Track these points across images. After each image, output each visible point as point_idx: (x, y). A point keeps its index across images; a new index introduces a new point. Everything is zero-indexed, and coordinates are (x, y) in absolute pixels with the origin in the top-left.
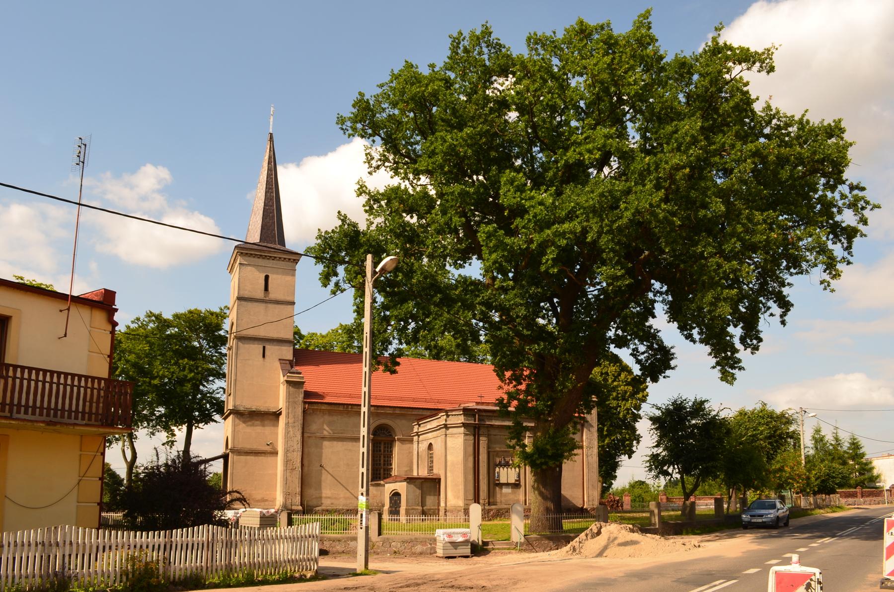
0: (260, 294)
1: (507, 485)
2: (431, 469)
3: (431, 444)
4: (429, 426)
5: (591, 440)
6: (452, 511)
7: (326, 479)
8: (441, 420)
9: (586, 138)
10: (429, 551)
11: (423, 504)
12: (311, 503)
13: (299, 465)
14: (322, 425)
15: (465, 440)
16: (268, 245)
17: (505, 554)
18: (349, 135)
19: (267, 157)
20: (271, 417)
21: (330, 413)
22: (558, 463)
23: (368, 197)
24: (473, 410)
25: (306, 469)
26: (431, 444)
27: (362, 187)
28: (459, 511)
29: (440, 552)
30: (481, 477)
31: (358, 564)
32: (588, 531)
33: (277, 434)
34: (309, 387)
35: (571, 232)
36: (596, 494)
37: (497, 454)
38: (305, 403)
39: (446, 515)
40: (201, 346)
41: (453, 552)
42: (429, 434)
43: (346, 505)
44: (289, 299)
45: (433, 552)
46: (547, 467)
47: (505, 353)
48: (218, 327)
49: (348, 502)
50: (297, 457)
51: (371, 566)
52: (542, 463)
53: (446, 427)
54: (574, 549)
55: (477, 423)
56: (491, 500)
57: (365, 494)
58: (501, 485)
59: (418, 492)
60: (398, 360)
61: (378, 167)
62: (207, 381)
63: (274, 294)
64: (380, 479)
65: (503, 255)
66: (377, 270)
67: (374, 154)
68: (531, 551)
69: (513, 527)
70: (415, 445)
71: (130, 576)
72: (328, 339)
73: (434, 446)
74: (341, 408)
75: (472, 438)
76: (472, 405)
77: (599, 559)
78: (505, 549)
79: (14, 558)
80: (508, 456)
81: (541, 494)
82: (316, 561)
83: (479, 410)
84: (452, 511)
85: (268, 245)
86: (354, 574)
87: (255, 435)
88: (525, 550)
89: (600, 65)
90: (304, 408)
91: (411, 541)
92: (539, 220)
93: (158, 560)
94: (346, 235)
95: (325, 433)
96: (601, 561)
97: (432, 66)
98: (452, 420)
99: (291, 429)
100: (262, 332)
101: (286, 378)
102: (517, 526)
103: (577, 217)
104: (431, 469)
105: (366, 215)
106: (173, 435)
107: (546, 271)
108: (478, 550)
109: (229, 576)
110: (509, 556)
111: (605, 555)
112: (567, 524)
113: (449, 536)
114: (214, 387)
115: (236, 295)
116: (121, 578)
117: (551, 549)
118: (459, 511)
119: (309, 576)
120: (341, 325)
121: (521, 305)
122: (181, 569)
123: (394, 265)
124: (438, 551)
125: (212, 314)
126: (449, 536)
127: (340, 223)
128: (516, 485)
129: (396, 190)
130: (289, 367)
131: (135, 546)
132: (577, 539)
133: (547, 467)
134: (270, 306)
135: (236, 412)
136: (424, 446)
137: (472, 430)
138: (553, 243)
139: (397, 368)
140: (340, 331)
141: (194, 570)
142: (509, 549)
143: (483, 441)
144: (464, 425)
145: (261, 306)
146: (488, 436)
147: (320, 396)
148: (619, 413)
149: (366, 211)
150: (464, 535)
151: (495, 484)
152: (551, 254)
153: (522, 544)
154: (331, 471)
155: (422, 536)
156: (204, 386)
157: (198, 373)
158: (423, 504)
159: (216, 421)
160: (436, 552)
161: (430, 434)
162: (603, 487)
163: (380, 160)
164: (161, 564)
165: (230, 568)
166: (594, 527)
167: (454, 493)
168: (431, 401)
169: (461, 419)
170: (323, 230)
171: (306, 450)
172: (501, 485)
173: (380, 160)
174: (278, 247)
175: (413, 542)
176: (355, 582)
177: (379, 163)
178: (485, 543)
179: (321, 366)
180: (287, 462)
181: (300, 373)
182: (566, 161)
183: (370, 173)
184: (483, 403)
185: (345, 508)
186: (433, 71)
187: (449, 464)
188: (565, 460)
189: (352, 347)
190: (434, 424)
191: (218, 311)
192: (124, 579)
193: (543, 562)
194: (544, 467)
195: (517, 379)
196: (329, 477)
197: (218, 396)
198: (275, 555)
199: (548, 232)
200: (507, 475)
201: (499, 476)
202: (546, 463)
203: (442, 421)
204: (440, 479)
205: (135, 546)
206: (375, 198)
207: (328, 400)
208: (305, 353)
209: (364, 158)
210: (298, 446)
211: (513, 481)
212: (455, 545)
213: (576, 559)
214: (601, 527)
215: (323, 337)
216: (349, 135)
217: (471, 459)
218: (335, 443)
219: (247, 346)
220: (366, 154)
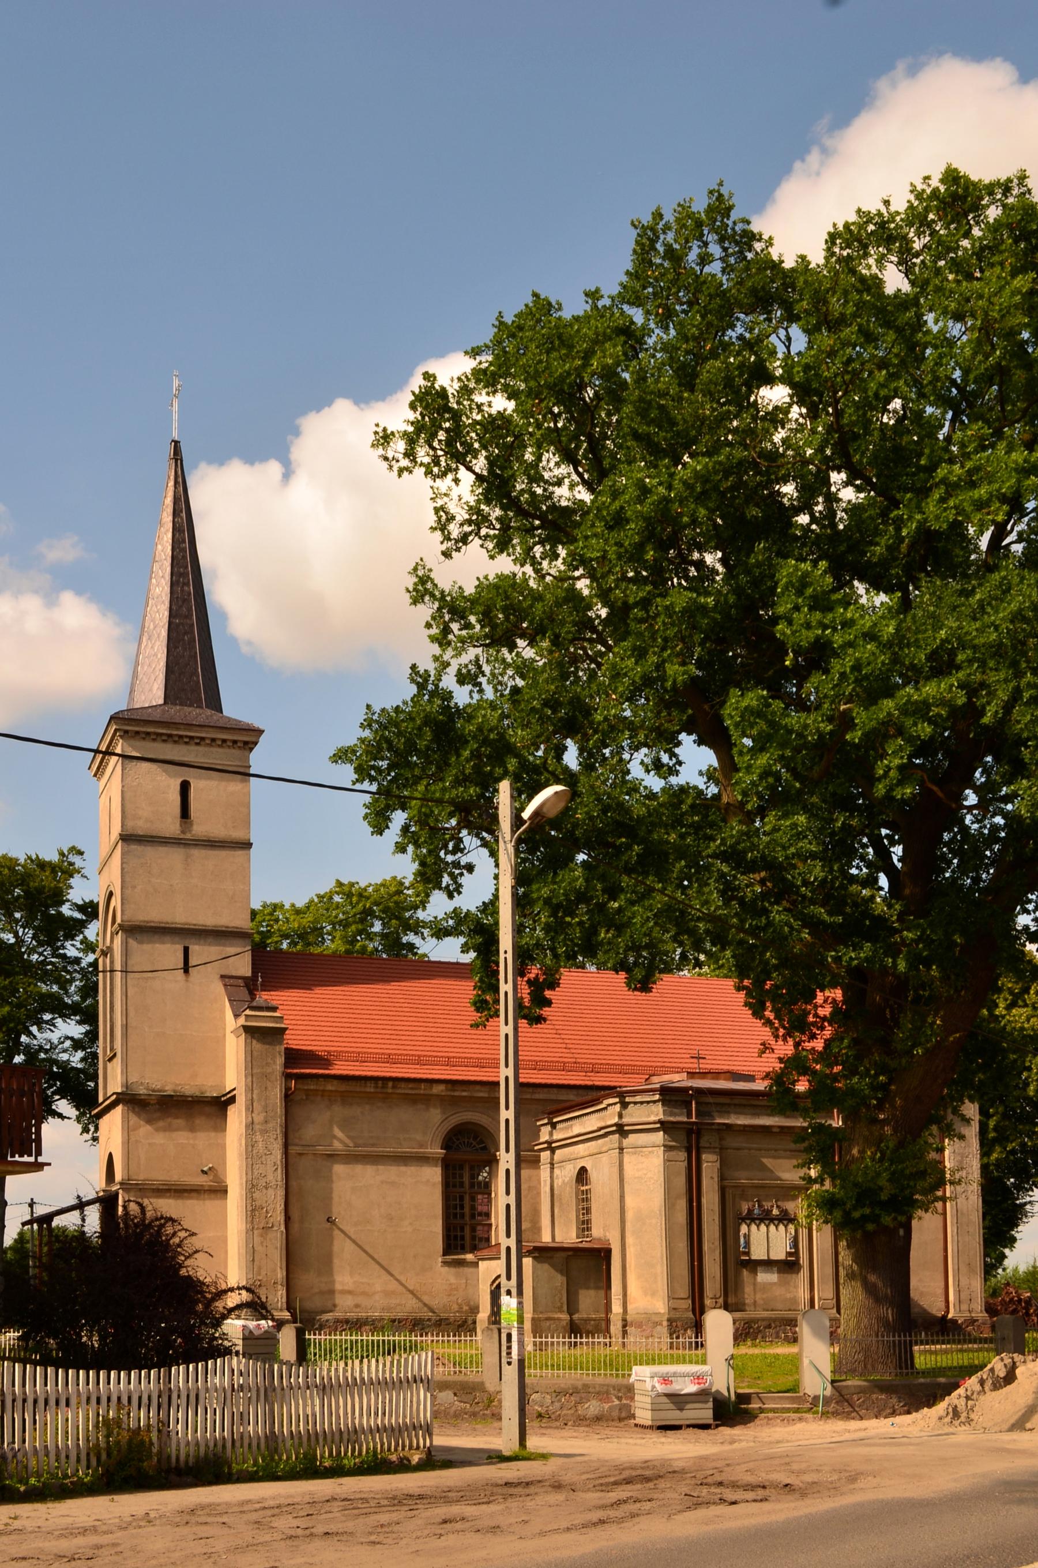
0: (171, 826)
1: (768, 1264)
2: (585, 1226)
3: (583, 1171)
4: (577, 1128)
5: (964, 1156)
6: (639, 1325)
7: (343, 1250)
8: (609, 1114)
9: (970, 473)
10: (615, 1414)
11: (572, 1307)
12: (309, 1305)
13: (280, 1218)
14: (330, 1128)
15: (666, 1161)
16: (188, 716)
17: (790, 1421)
18: (401, 471)
19: (169, 500)
20: (208, 1109)
21: (346, 1098)
22: (902, 1219)
23: (436, 605)
24: (684, 1090)
25: (295, 1227)
26: (583, 1171)
27: (424, 580)
28: (657, 1324)
29: (644, 1415)
30: (706, 1247)
31: (505, 1440)
32: (984, 1373)
33: (223, 1147)
34: (294, 1040)
35: (942, 702)
36: (976, 1285)
37: (743, 1192)
38: (288, 1077)
39: (625, 1333)
40: (20, 941)
41: (674, 1416)
42: (579, 1142)
43: (389, 1309)
44: (237, 834)
45: (624, 1416)
46: (876, 1229)
47: (767, 962)
48: (58, 897)
49: (393, 1301)
50: (274, 1201)
51: (534, 1443)
52: (864, 1218)
53: (621, 1130)
54: (956, 1414)
55: (697, 1120)
56: (731, 1300)
57: (514, 1291)
58: (754, 1265)
59: (560, 1280)
60: (548, 993)
61: (464, 539)
62: (39, 1023)
63: (202, 826)
64: (463, 1250)
65: (782, 757)
66: (526, 815)
67: (453, 508)
68: (847, 1416)
69: (806, 1362)
70: (544, 1172)
71: (104, 1456)
72: (309, 917)
73: (593, 1174)
74: (370, 1088)
75: (683, 1155)
76: (678, 1079)
77: (1016, 1435)
78: (788, 1410)
79: (24, 1420)
80: (768, 1198)
81: (870, 1290)
82: (428, 1430)
83: (700, 1092)
84: (639, 1325)
85: (188, 716)
86: (497, 1457)
87: (172, 1151)
88: (835, 1414)
89: (1003, 300)
90: (287, 1089)
91: (575, 1391)
92: (866, 677)
93: (149, 1425)
94: (428, 720)
95: (337, 1145)
96: (1022, 1439)
97: (593, 295)
98: (635, 1115)
99: (258, 1137)
100: (180, 916)
101: (242, 1021)
102: (815, 1358)
103: (959, 668)
104: (585, 1226)
105: (436, 649)
107: (889, 797)
108: (731, 1411)
109: (272, 1459)
110: (799, 1426)
111: (1028, 1426)
112: (927, 1356)
113: (666, 1380)
114: (55, 1037)
115: (117, 830)
116: (88, 1460)
117: (894, 1413)
118: (657, 1324)
119: (415, 1459)
120: (340, 884)
121: (813, 856)
122: (188, 1443)
123: (561, 805)
124: (638, 1413)
125: (42, 865)
126: (666, 1380)
127: (413, 689)
128: (789, 1266)
129: (505, 586)
130: (244, 993)
131: (109, 1399)
132: (961, 1391)
133: (876, 1229)
134: (196, 853)
135: (128, 1099)
136: (566, 1174)
137: (683, 1136)
138: (900, 732)
139: (546, 1012)
140: (337, 899)
141: (211, 1444)
142: (797, 1411)
143: (710, 1164)
144: (664, 1126)
145: (174, 857)
146: (722, 1151)
147: (325, 1061)
148: (1027, 1084)
149: (433, 639)
150: (698, 1378)
151: (739, 1263)
152: (894, 758)
153: (827, 1401)
154: (351, 1231)
155: (600, 1380)
156: (30, 1034)
157: (19, 1006)
158: (572, 1307)
159: (61, 1116)
160: (633, 1416)
161: (580, 1147)
162: (986, 1264)
163: (469, 522)
164: (154, 1436)
165: (272, 1441)
166: (998, 1365)
167: (643, 1284)
168: (576, 1067)
169: (657, 1113)
170: (377, 708)
171: (293, 1183)
172: (754, 1265)
173: (469, 522)
174: (204, 715)
175: (580, 1393)
176: (521, 1474)
177: (467, 529)
178: (744, 1398)
179: (318, 990)
180: (253, 1211)
181: (274, 1009)
182: (921, 524)
183: (447, 554)
184: (704, 1075)
185: (387, 1315)
186: (595, 307)
187: (629, 1215)
188: (920, 1212)
189: (370, 937)
190: (591, 1123)
191: (53, 857)
192: (94, 1462)
193: (891, 1440)
194: (870, 1227)
195: (798, 1026)
196: (349, 1246)
197: (64, 1057)
198: (338, 1417)
199: (888, 704)
200: (767, 1241)
201: (748, 1244)
202: (875, 1219)
203: (611, 1117)
204: (608, 1252)
205: (109, 1399)
206: (453, 608)
207: (340, 1068)
208: (278, 958)
209: (432, 519)
210: (276, 1177)
212: (678, 1400)
213: (962, 1435)
214: (1014, 1366)
215: (298, 912)
216: (401, 471)
217: (682, 1204)
218: (359, 1168)
219: (147, 947)
220: (437, 510)
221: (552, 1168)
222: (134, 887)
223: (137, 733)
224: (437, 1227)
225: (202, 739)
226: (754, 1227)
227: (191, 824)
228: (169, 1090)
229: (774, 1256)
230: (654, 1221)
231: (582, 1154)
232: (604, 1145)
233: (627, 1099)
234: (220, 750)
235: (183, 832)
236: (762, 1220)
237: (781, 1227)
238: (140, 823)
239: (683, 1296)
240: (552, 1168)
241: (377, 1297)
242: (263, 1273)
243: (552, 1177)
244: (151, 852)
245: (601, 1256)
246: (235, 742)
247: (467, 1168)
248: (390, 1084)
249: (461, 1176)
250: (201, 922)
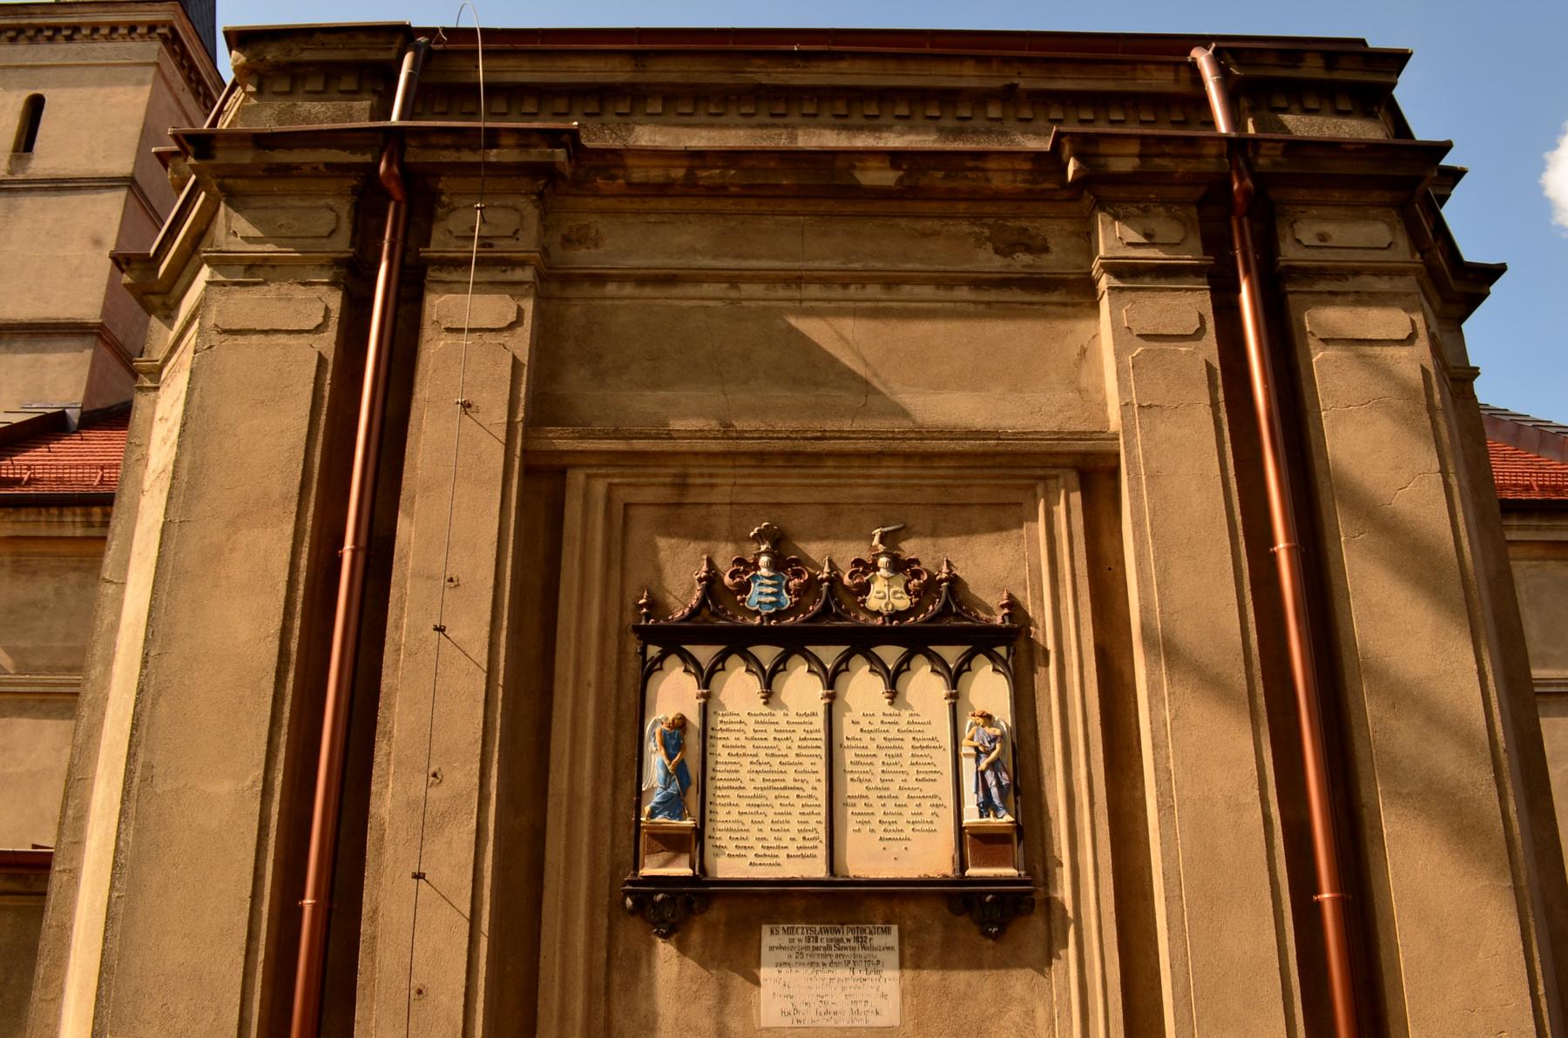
1: (836, 906)
211: (931, 856)
229: (867, 859)
234: (109, 45)
236: (794, 640)
237: (925, 684)
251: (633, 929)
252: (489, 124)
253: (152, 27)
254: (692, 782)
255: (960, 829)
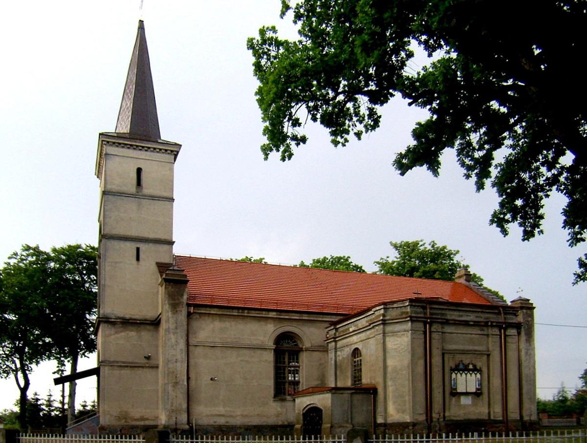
0: (143, 247)
1: (467, 394)
20: (148, 327)
70: (332, 355)
106: (64, 365)
211: (474, 390)
221: (336, 352)
222: (110, 218)
223: (114, 143)
224: (271, 383)
225: (149, 148)
226: (459, 375)
227: (142, 189)
228: (128, 317)
229: (469, 390)
230: (404, 372)
231: (355, 341)
232: (371, 334)
233: (388, 307)
234: (158, 154)
235: (137, 192)
236: (463, 371)
237: (473, 375)
238: (114, 187)
239: (422, 412)
240: (336, 352)
241: (238, 418)
242: (174, 405)
243: (335, 356)
244: (119, 201)
245: (372, 391)
246: (166, 150)
247: (287, 354)
248: (246, 311)
249: (284, 358)
250: (146, 236)
251: (451, 396)
252: (428, 313)
253: (172, 151)
254: (456, 384)
255: (476, 388)
